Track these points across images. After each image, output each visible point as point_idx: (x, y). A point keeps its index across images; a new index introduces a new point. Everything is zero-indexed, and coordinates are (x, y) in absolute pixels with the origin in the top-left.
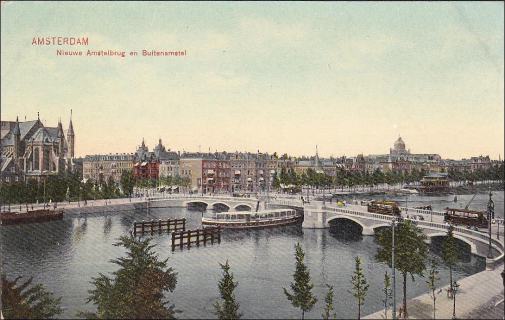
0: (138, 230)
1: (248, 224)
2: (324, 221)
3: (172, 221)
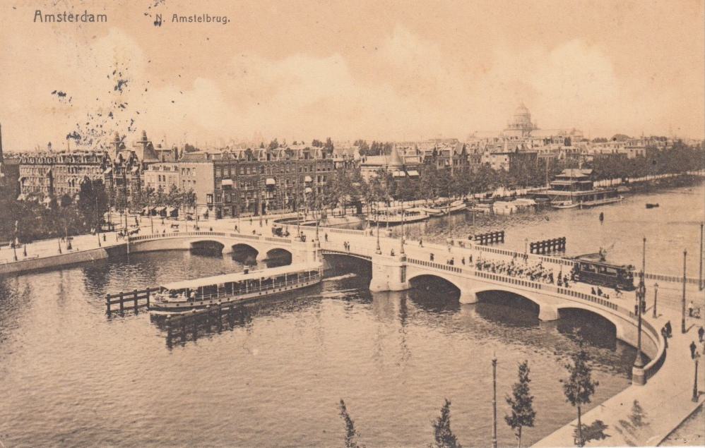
0: (113, 307)
1: (229, 302)
2: (403, 280)
3: (115, 297)
